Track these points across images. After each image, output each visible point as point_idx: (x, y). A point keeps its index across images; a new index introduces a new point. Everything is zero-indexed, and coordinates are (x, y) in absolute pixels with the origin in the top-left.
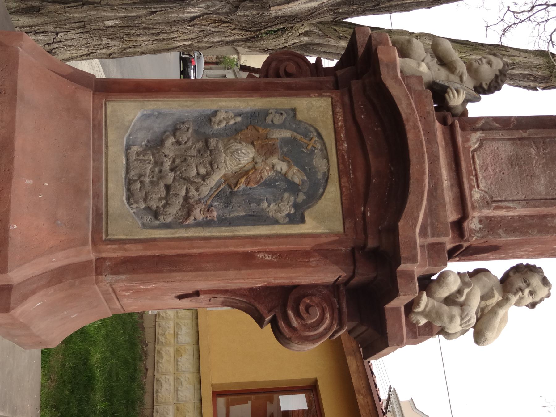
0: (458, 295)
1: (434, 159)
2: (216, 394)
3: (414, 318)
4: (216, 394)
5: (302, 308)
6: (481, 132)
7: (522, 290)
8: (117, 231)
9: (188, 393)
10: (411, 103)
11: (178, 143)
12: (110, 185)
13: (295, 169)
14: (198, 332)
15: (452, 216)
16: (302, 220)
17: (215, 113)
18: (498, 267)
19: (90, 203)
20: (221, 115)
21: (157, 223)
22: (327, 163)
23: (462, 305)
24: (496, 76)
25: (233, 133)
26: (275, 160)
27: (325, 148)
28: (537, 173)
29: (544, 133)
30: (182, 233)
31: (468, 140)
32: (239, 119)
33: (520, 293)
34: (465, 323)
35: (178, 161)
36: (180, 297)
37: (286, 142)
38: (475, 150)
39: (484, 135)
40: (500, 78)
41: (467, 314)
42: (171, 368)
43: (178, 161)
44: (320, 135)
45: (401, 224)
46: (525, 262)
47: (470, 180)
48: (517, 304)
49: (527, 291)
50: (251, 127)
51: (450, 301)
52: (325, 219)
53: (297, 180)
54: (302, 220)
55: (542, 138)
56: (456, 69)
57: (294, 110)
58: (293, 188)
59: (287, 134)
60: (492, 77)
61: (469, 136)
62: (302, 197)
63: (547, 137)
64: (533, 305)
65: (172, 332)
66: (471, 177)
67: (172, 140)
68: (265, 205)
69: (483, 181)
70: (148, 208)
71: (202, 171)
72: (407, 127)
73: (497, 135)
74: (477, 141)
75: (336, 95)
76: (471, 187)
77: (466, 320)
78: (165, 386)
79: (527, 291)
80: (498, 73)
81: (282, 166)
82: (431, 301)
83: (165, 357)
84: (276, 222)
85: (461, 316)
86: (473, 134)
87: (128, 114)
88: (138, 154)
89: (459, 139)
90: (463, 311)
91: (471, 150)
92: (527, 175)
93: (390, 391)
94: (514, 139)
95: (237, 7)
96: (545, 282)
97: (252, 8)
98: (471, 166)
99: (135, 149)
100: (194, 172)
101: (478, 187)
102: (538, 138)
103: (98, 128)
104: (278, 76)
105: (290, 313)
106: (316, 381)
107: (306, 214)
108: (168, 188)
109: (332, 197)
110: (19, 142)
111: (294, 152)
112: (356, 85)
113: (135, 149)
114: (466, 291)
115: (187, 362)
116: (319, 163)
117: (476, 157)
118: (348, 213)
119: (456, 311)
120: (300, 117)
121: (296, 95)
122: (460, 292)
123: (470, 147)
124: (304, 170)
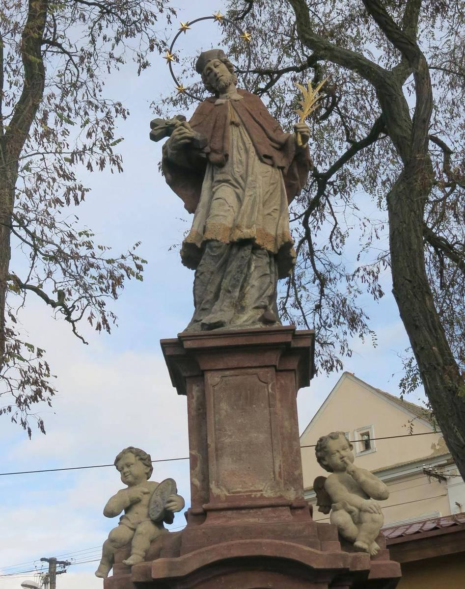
0: (353, 514)
1: (248, 531)
6: (210, 484)
7: (342, 458)
10: (206, 551)
15: (286, 513)
23: (360, 510)
24: (141, 459)
28: (248, 438)
31: (218, 496)
33: (345, 459)
34: (377, 510)
38: (229, 491)
39: (214, 482)
40: (143, 457)
41: (371, 508)
45: (315, 566)
47: (255, 498)
51: (358, 522)
55: (215, 431)
56: (138, 498)
61: (215, 496)
63: (215, 427)
66: (253, 496)
69: (256, 486)
72: (229, 556)
73: (213, 468)
74: (219, 488)
76: (262, 497)
77: (375, 509)
79: (343, 453)
80: (138, 458)
85: (372, 513)
86: (213, 491)
89: (220, 505)
90: (366, 511)
91: (228, 495)
92: (250, 448)
94: (217, 455)
96: (333, 437)
98: (243, 496)
101: (261, 491)
102: (215, 434)
114: (349, 507)
117: (233, 491)
119: (366, 517)
122: (350, 512)
123: (226, 496)
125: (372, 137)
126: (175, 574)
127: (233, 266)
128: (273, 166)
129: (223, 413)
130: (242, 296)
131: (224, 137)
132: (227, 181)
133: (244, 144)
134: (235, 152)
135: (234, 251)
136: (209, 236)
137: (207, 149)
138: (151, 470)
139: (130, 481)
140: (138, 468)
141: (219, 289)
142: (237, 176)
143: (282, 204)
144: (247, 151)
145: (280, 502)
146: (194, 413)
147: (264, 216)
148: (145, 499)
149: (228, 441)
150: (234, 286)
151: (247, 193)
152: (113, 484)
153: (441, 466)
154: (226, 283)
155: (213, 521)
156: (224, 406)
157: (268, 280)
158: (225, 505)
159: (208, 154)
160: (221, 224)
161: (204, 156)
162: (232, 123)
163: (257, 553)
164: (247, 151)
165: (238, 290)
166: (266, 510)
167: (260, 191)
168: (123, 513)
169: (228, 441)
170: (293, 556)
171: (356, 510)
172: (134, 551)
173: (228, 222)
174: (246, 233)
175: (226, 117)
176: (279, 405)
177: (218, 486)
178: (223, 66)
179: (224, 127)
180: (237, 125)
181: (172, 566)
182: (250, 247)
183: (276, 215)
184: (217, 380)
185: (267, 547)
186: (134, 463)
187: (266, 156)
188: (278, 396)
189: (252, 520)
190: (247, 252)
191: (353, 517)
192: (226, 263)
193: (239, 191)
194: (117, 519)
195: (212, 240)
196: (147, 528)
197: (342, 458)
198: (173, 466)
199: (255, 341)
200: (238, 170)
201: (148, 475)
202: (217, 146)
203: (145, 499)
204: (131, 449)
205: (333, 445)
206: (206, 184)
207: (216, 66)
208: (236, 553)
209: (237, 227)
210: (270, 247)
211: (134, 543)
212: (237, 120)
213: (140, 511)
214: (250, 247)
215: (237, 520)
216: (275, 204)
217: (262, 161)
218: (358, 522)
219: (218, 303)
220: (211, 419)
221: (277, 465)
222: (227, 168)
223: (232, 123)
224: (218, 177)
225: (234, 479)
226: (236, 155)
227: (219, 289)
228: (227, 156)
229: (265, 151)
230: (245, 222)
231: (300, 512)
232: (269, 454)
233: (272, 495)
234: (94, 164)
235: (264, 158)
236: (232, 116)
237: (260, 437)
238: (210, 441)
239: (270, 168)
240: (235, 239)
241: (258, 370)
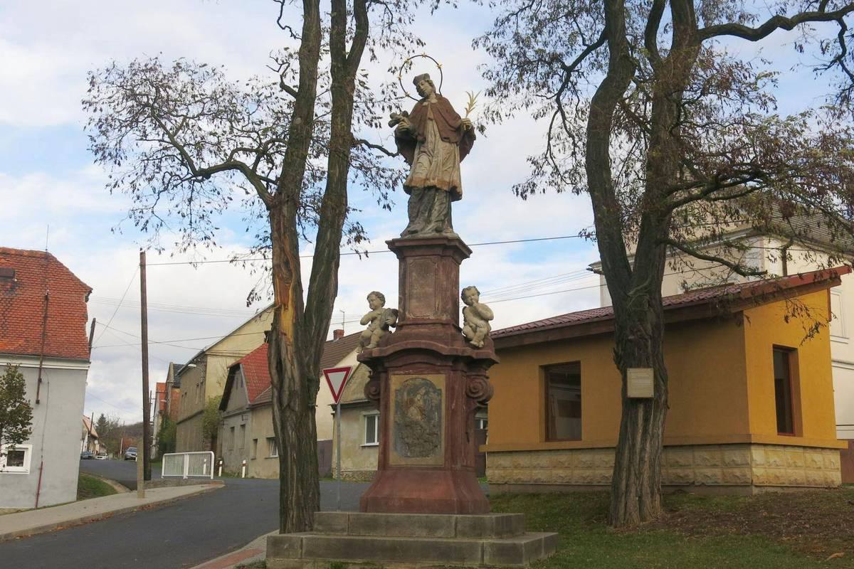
2: (548, 439)
3: (481, 346)
4: (548, 439)
5: (474, 391)
7: (472, 299)
8: (441, 462)
9: (544, 460)
11: (407, 437)
12: (423, 463)
13: (420, 391)
14: (503, 452)
15: (439, 328)
16: (440, 390)
17: (396, 422)
18: (462, 304)
19: (430, 472)
20: (397, 419)
21: (439, 446)
22: (418, 379)
23: (477, 326)
24: (379, 297)
25: (404, 415)
26: (416, 399)
27: (412, 379)
29: (408, 284)
30: (443, 437)
31: (409, 318)
32: (399, 413)
35: (414, 437)
36: (468, 441)
37: (408, 394)
42: (528, 472)
43: (414, 437)
44: (407, 381)
46: (460, 295)
48: (477, 301)
49: (473, 297)
50: (403, 407)
51: (475, 331)
52: (439, 380)
53: (424, 391)
54: (440, 390)
57: (396, 390)
58: (427, 393)
59: (405, 394)
60: (378, 299)
62: (431, 390)
64: (479, 293)
65: (502, 472)
67: (406, 439)
68: (433, 404)
70: (433, 449)
71: (419, 428)
75: (390, 373)
76: (429, 319)
78: (539, 476)
79: (473, 297)
81: (418, 397)
82: (474, 339)
83: (520, 476)
84: (441, 400)
87: (395, 458)
88: (411, 453)
89: (409, 323)
93: (592, 270)
95: (293, 410)
97: (295, 401)
99: (409, 454)
100: (419, 431)
103: (399, 468)
104: (379, 394)
105: (476, 396)
106: (541, 367)
107: (437, 388)
108: (425, 442)
109: (430, 377)
110: (407, 497)
111: (414, 390)
112: (387, 365)
113: (409, 454)
114: (471, 324)
115: (524, 460)
116: (418, 382)
118: (438, 372)
119: (478, 329)
120: (399, 388)
121: (389, 389)
122: (471, 327)
124: (420, 388)
125: (600, 43)
126: (383, 355)
127: (426, 199)
128: (450, 142)
129: (414, 278)
130: (430, 216)
131: (425, 127)
132: (425, 152)
133: (434, 131)
134: (429, 136)
135: (426, 192)
136: (413, 184)
137: (416, 133)
138: (384, 302)
139: (374, 307)
140: (377, 302)
141: (418, 212)
142: (430, 149)
143: (454, 164)
144: (435, 136)
145: (437, 321)
146: (401, 277)
147: (443, 172)
148: (379, 317)
149: (415, 291)
150: (426, 211)
151: (434, 160)
152: (366, 309)
153: (742, 239)
154: (422, 208)
155: (405, 330)
156: (414, 274)
157: (444, 206)
158: (411, 322)
159: (417, 136)
160: (420, 178)
161: (414, 137)
162: (429, 119)
163: (418, 347)
164: (435, 136)
165: (427, 213)
166: (430, 325)
167: (440, 158)
168: (370, 322)
169: (415, 291)
170: (434, 348)
171: (474, 326)
172: (372, 342)
173: (423, 176)
174: (431, 182)
175: (426, 115)
176: (441, 273)
177: (409, 313)
178: (427, 84)
179: (425, 121)
180: (432, 120)
181: (381, 351)
182: (434, 189)
183: (450, 170)
184: (412, 261)
185: (423, 344)
186: (376, 299)
187: (445, 138)
188: (441, 269)
189: (422, 330)
190: (433, 192)
191: (472, 329)
192: (421, 199)
193: (430, 158)
194: (367, 326)
195: (414, 187)
196: (378, 331)
197: (472, 299)
198: (392, 302)
199: (429, 243)
200: (430, 146)
201: (383, 305)
202: (421, 133)
203: (379, 317)
204: (373, 293)
205: (468, 293)
206: (416, 152)
207: (422, 85)
208: (398, 349)
209: (427, 179)
210: (446, 188)
211: (372, 338)
212: (432, 117)
213: (377, 322)
214: (434, 189)
215: (416, 330)
216: (450, 164)
217: (442, 140)
218: (475, 331)
219: (418, 219)
220: (408, 281)
221: (437, 303)
222: (426, 145)
223: (429, 119)
224: (422, 150)
225: (419, 310)
226: (430, 138)
227: (418, 212)
228: (425, 138)
229: (444, 135)
230: (432, 176)
231: (447, 326)
232: (433, 299)
233: (433, 318)
234: (386, 108)
235: (444, 139)
236: (430, 114)
237: (430, 290)
238: (407, 292)
239: (448, 144)
240: (426, 186)
241: (431, 257)
